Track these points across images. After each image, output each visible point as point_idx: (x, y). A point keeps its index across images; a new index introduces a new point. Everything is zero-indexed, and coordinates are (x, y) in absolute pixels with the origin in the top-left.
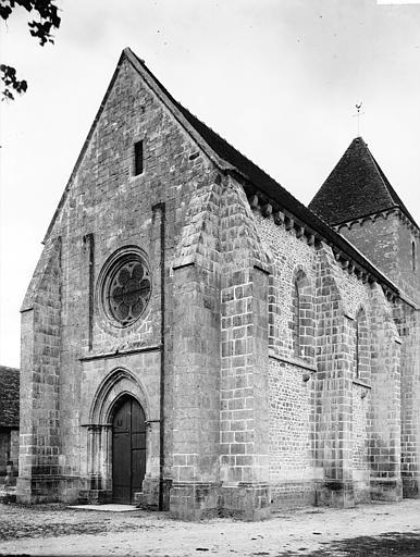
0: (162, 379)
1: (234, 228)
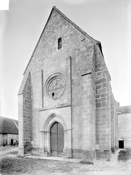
0: (72, 116)
1: (104, 74)
